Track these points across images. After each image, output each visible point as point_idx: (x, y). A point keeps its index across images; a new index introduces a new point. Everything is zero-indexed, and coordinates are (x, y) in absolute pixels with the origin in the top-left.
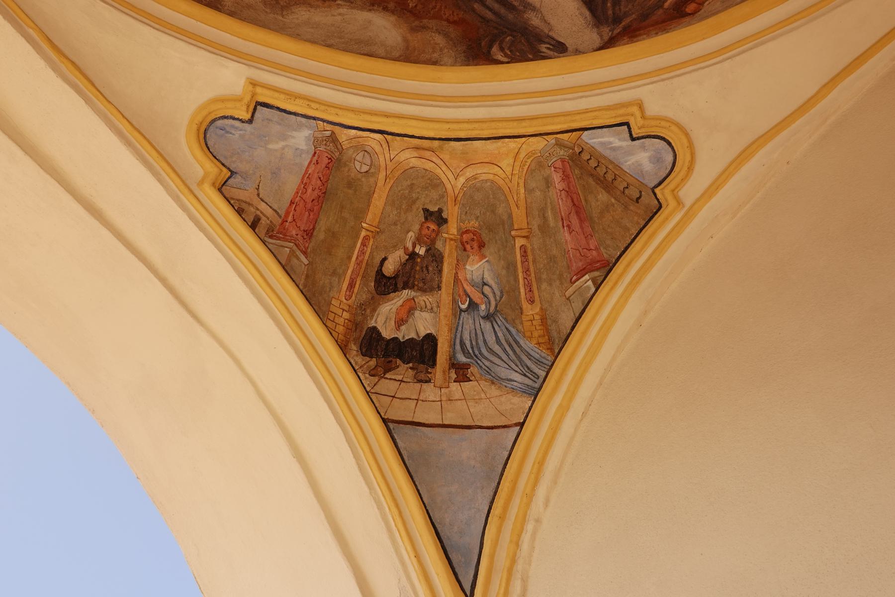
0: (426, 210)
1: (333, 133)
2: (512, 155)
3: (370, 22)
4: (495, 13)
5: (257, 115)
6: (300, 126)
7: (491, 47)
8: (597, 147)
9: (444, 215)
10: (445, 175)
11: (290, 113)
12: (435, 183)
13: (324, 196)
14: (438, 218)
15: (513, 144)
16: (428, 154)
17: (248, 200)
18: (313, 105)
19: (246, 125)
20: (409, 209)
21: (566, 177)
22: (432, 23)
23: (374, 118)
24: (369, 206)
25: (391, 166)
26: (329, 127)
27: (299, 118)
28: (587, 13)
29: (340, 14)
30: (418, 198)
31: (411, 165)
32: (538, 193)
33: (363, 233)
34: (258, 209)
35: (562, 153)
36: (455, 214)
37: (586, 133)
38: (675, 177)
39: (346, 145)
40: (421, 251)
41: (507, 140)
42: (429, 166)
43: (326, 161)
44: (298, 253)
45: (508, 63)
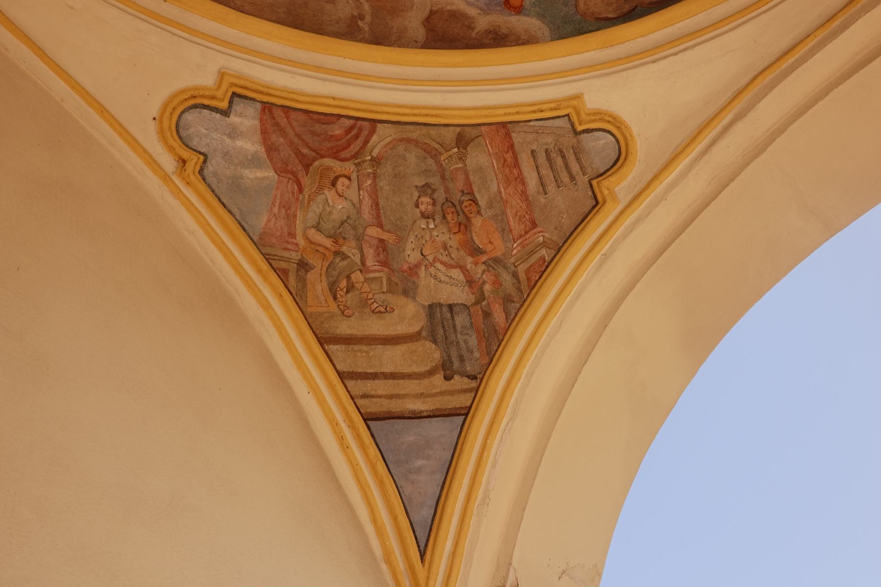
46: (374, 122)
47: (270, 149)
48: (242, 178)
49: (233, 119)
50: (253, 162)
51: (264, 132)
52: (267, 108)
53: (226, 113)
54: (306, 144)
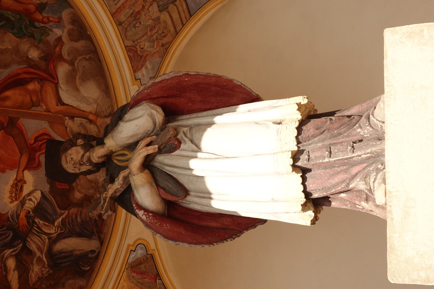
7: (81, 269)
28: (84, 238)
32: (134, 281)
46: (126, 47)
47: (142, 66)
48: (151, 68)
49: (140, 77)
52: (134, 72)
53: (140, 79)
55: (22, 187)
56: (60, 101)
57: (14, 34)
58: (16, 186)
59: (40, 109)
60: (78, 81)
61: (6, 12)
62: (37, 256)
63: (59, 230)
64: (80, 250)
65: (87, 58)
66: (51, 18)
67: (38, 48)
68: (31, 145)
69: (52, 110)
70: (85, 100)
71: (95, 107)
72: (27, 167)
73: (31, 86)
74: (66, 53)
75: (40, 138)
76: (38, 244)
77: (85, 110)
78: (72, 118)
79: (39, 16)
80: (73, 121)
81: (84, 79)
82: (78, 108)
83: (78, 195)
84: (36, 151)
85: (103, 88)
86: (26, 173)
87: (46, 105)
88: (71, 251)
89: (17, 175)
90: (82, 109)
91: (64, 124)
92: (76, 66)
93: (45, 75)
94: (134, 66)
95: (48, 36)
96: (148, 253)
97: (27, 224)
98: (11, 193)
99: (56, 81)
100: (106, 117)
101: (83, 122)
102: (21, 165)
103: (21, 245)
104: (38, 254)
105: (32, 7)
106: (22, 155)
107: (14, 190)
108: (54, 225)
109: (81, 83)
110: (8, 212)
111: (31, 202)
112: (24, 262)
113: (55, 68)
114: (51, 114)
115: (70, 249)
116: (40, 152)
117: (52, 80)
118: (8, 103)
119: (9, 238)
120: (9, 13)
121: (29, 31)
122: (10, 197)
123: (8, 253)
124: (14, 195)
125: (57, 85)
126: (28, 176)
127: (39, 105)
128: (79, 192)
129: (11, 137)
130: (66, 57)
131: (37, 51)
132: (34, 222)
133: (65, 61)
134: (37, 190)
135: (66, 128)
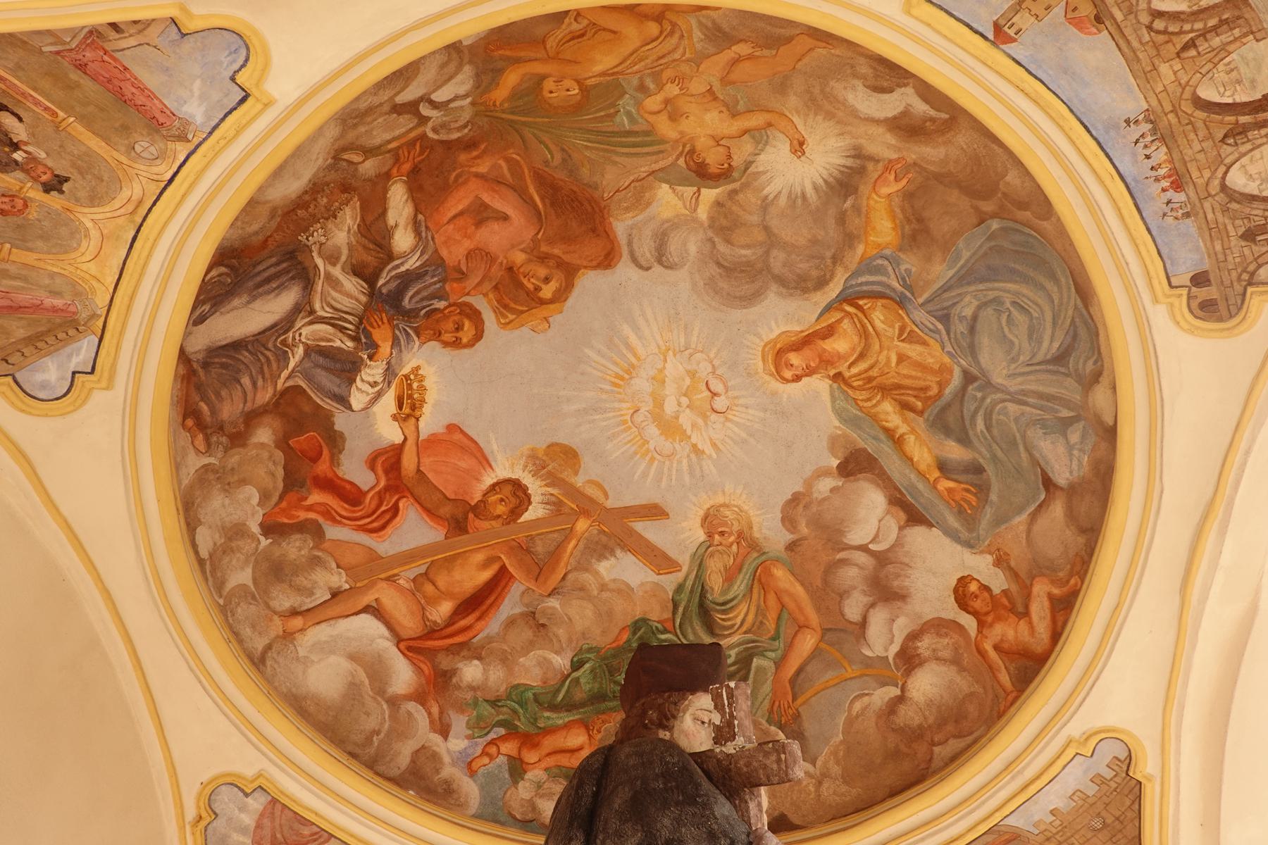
0: (67, 180)
1: (189, 141)
2: (99, 276)
3: (299, 178)
4: (259, 273)
5: (237, 88)
6: (209, 118)
7: (226, 266)
8: (78, 344)
9: (54, 193)
10: (100, 213)
11: (226, 116)
12: (94, 199)
13: (122, 99)
14: (55, 184)
15: (110, 280)
16: (130, 207)
17: (145, 32)
18: (223, 142)
19: (231, 73)
20: (74, 165)
21: (55, 310)
22: (274, 224)
23: (186, 185)
24: (94, 133)
25: (130, 171)
26: (196, 141)
27: (217, 121)
28: (224, 343)
29: (317, 159)
30: (84, 178)
31: (124, 189)
32: (47, 281)
33: (61, 114)
34: (131, 36)
35: (84, 315)
36: (52, 204)
37: (97, 340)
38: (15, 393)
39: (171, 145)
40: (18, 156)
41: (117, 277)
42: (117, 203)
43: (161, 120)
44: (59, 48)
45: (203, 280)
46: (331, 836)
47: (259, 826)
48: (229, 837)
49: (250, 800)
50: (243, 830)
51: (262, 815)
52: (274, 801)
53: (247, 795)
54: (282, 832)
55: (400, 406)
56: (375, 610)
57: (528, 687)
58: (414, 405)
59: (407, 575)
60: (362, 676)
61: (567, 720)
62: (339, 267)
63: (290, 339)
64: (232, 310)
65: (375, 738)
66: (486, 760)
67: (472, 688)
68: (404, 497)
69: (384, 584)
70: (326, 648)
71: (299, 648)
72: (398, 450)
73: (446, 608)
74: (416, 715)
75: (387, 517)
76: (340, 292)
77: (318, 627)
78: (335, 594)
79: (509, 748)
80: (330, 588)
81: (353, 688)
82: (332, 622)
83: (264, 435)
84: (387, 489)
85: (308, 702)
86: (397, 438)
87: (400, 589)
88: (254, 298)
89: (417, 428)
90: (323, 625)
91: (345, 570)
92: (383, 703)
93: (430, 644)
94: (282, 811)
95: (468, 723)
96: (9, 379)
97: (371, 330)
98: (422, 389)
99: (402, 645)
100: (269, 647)
101: (308, 600)
102: (414, 448)
103: (381, 282)
104: (336, 272)
105: (530, 757)
106: (419, 471)
107: (416, 396)
108: (306, 345)
109: (353, 676)
110: (420, 347)
111: (371, 379)
112: (371, 246)
113: (418, 670)
114: (383, 576)
115: (257, 304)
116: (377, 489)
117: (411, 643)
118: (480, 557)
119: (410, 293)
120: (560, 722)
121: (505, 709)
122: (421, 379)
123: (411, 262)
124: (415, 385)
125: (399, 640)
126: (391, 433)
127: (414, 580)
128: (263, 445)
129: (453, 497)
130: (412, 706)
131: (469, 679)
132: (355, 339)
133: (409, 697)
134: (363, 410)
135: (338, 567)
